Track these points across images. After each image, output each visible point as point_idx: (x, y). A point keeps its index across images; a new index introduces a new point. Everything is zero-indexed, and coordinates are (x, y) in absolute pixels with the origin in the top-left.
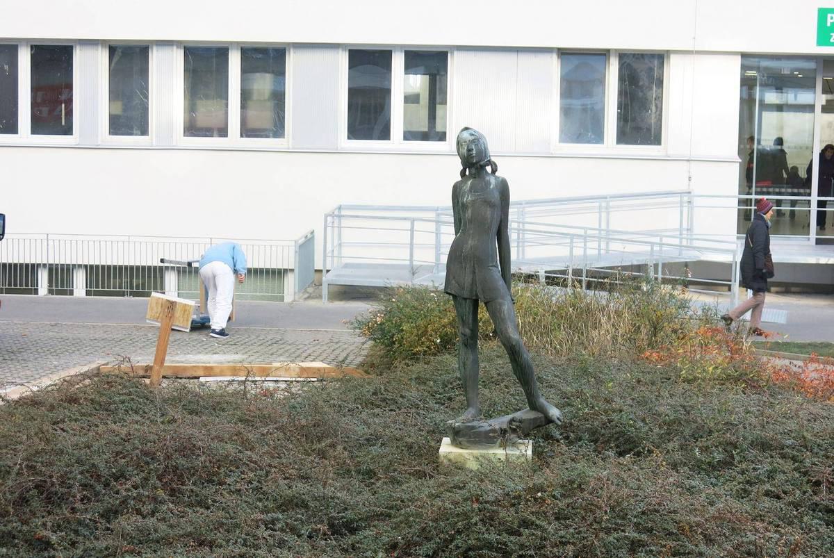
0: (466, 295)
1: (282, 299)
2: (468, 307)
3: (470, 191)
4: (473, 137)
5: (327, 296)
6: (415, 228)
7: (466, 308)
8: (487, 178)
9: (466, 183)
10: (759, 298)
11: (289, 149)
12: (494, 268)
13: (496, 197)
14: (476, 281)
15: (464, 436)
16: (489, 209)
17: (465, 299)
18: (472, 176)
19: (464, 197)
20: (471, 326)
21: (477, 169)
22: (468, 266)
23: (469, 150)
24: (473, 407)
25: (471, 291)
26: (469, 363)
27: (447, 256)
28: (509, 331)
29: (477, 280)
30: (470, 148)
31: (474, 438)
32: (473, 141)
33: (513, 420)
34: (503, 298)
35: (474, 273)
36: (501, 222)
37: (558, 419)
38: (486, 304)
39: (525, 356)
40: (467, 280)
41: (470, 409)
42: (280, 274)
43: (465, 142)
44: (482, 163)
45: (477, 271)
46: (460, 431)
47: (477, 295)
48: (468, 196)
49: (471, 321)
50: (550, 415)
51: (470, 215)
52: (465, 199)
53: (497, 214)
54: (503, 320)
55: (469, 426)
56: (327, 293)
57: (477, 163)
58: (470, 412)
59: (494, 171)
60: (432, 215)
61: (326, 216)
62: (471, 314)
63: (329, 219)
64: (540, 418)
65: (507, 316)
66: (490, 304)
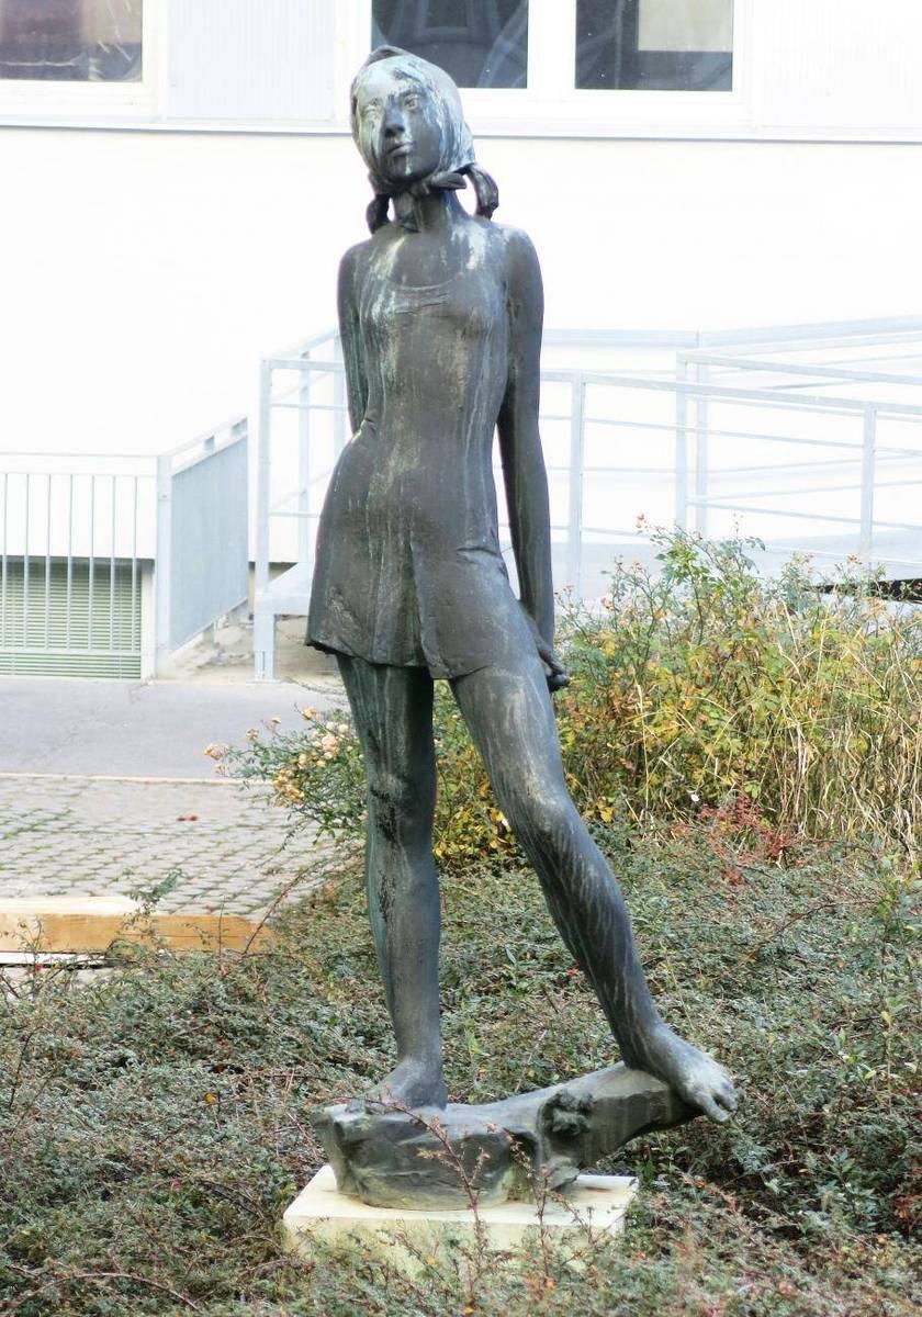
0: (381, 652)
1: (132, 669)
2: (391, 696)
3: (396, 278)
4: (404, 85)
5: (270, 657)
6: (589, 412)
7: (382, 701)
8: (459, 232)
9: (383, 250)
10: (417, 644)
11: (154, 120)
12: (481, 557)
13: (487, 300)
14: (415, 600)
15: (374, 1160)
16: (460, 343)
17: (380, 668)
18: (409, 225)
19: (375, 300)
20: (404, 763)
21: (420, 198)
22: (388, 548)
23: (390, 132)
24: (419, 1059)
25: (400, 637)
26: (400, 895)
27: (552, 523)
28: (529, 784)
29: (420, 599)
30: (391, 123)
31: (408, 1168)
32: (404, 100)
33: (556, 1104)
34: (510, 663)
35: (409, 572)
36: (510, 389)
37: (719, 1100)
38: (454, 682)
39: (592, 872)
40: (386, 595)
41: (407, 1063)
42: (127, 575)
43: (375, 102)
44: (438, 177)
45: (419, 566)
46: (361, 1141)
47: (419, 653)
48: (388, 296)
49: (402, 749)
50: (690, 1086)
51: (394, 365)
52: (376, 310)
53: (493, 367)
54: (510, 745)
55: (392, 1125)
56: (270, 649)
57: (417, 177)
58: (405, 1072)
59: (486, 209)
60: (663, 363)
61: (269, 367)
62: (402, 719)
63: (286, 381)
64: (656, 1097)
65: (522, 729)
66: (464, 686)
